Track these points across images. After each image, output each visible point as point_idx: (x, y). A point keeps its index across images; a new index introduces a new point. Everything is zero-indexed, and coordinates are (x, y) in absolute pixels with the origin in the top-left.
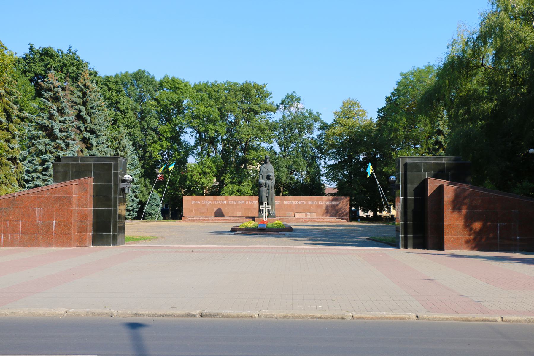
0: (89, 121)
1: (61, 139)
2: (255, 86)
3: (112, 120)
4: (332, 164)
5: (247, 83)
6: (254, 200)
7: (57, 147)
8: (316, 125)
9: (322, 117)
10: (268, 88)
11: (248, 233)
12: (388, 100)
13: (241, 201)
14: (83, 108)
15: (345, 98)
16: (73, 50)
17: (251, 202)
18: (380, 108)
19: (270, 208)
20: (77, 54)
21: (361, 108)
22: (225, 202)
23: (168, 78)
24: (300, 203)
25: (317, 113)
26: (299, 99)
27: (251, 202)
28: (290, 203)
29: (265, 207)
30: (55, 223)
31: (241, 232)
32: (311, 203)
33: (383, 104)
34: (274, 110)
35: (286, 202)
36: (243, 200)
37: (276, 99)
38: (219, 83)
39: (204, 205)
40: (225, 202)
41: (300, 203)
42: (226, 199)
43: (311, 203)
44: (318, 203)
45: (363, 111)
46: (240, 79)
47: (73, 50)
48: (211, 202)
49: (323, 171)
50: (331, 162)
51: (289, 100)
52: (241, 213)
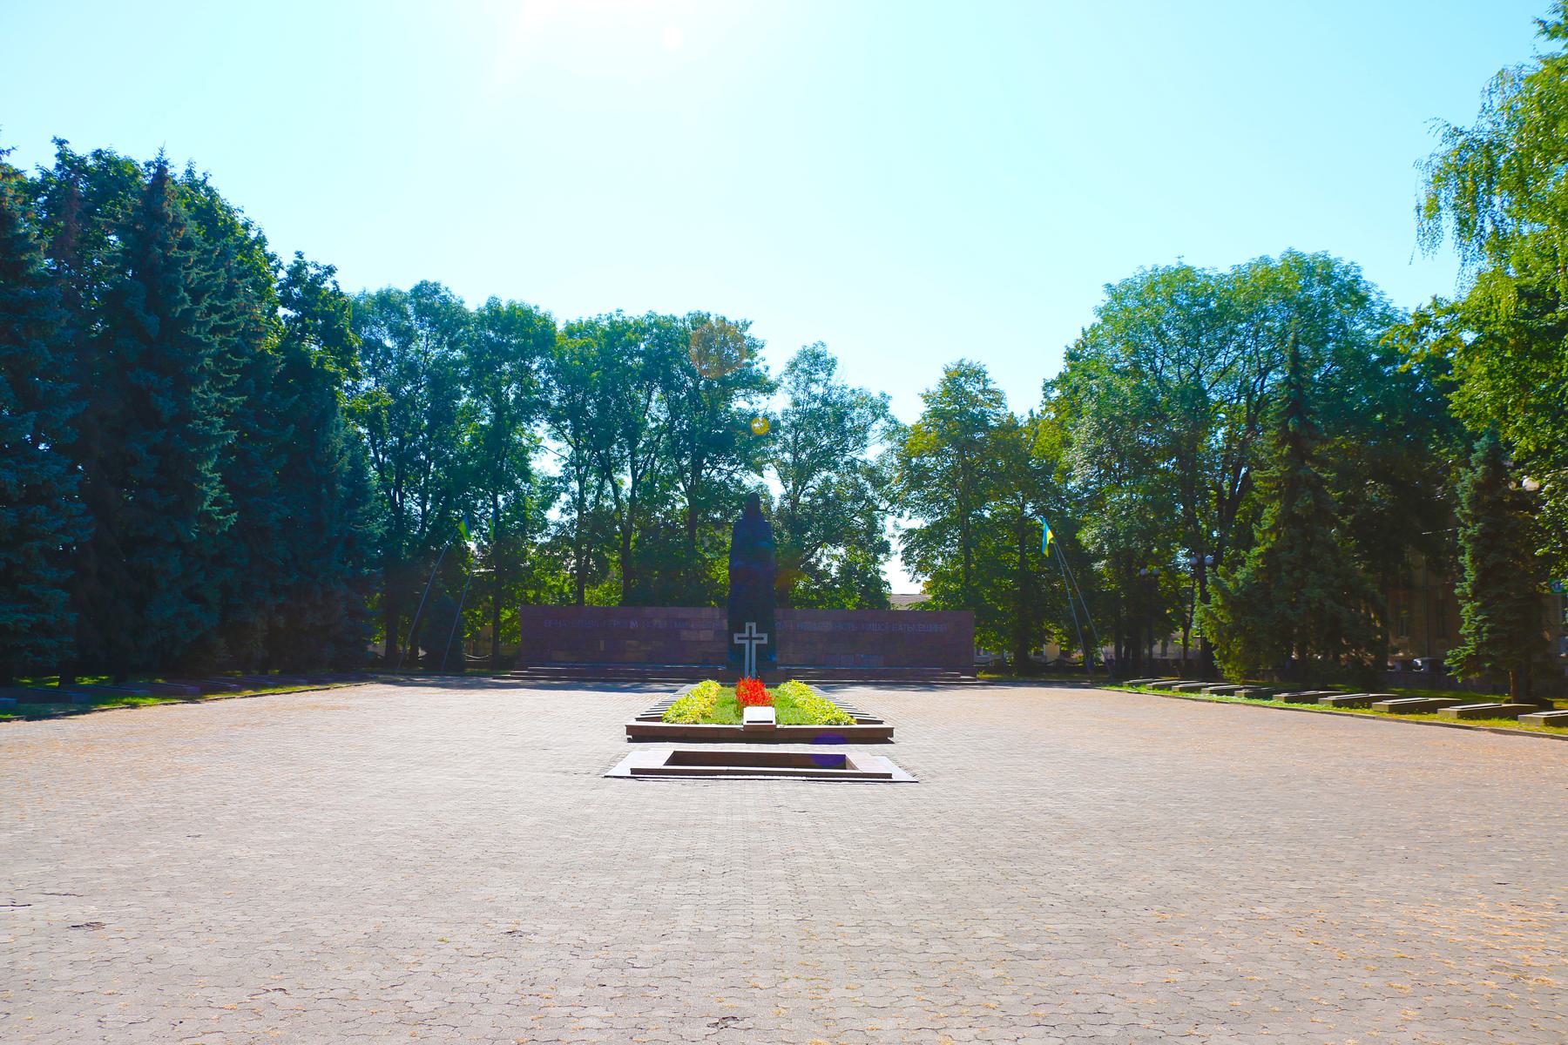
12: (1072, 356)
15: (951, 360)
18: (1053, 375)
21: (990, 386)
25: (883, 395)
26: (833, 362)
37: (773, 360)
50: (919, 523)
51: (814, 362)
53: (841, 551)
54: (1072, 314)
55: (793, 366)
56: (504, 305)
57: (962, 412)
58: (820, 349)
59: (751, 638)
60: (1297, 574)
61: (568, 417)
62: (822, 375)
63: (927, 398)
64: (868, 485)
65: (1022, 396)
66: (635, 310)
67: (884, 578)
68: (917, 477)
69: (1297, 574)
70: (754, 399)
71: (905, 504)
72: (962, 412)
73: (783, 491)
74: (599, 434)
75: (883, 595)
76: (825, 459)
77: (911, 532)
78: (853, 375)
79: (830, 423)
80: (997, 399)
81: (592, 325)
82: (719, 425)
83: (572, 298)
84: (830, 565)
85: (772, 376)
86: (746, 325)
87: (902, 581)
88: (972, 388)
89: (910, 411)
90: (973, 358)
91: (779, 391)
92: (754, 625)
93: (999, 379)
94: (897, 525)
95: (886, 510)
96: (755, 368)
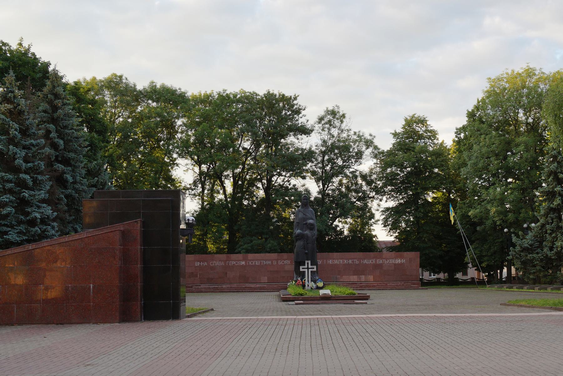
0: (62, 147)
1: (26, 173)
2: (283, 98)
3: (88, 146)
4: (391, 206)
5: (269, 92)
6: (285, 260)
7: (22, 184)
8: (368, 152)
9: (376, 142)
10: (300, 102)
11: (316, 302)
12: (471, 115)
13: (266, 260)
14: (52, 127)
15: (408, 114)
16: (26, 45)
17: (280, 263)
18: (460, 125)
19: (315, 270)
20: (32, 50)
21: (429, 128)
22: (243, 263)
23: (156, 86)
24: (350, 261)
25: (371, 135)
26: (344, 116)
27: (280, 263)
28: (336, 262)
29: (308, 268)
30: (93, 287)
31: (302, 302)
32: (366, 261)
33: (463, 121)
34: (305, 131)
35: (330, 262)
36: (269, 260)
37: (309, 116)
38: (228, 92)
39: (213, 268)
40: (243, 263)
41: (350, 261)
42: (245, 259)
43: (366, 261)
44: (376, 261)
45: (430, 131)
46: (260, 89)
47: (26, 45)
48: (223, 264)
49: (378, 216)
50: (391, 204)
51: (333, 117)
52: (266, 278)
53: (349, 220)
54: (472, 92)
55: (321, 119)
56: (158, 86)
57: (413, 135)
58: (336, 110)
59: (308, 268)
60: (554, 235)
61: (198, 151)
62: (337, 123)
63: (395, 135)
64: (364, 183)
65: (446, 131)
66: (233, 87)
67: (374, 233)
68: (390, 180)
69: (554, 235)
70: (299, 136)
71: (384, 193)
72: (413, 135)
73: (318, 189)
74: (213, 156)
75: (374, 242)
76: (340, 171)
77: (387, 209)
78: (356, 124)
79: (341, 151)
80: (433, 134)
81: (208, 96)
82: (296, 163)
83: (197, 81)
84: (344, 227)
85: (309, 126)
86: (295, 98)
87: (382, 234)
88: (420, 129)
89: (386, 143)
90: (420, 114)
91: (313, 134)
92: (309, 262)
93: (433, 124)
94: (380, 206)
95: (373, 197)
96: (300, 121)
